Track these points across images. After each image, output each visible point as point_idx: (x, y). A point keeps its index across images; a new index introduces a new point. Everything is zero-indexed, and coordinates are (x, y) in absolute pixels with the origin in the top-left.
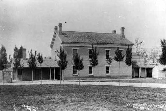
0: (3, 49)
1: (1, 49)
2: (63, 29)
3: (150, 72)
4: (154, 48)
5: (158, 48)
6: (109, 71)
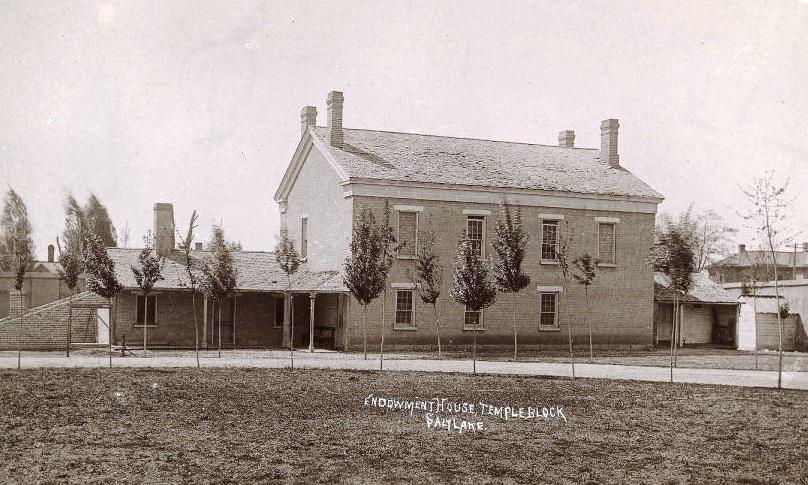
0: (16, 203)
1: (5, 200)
2: (349, 121)
3: (726, 324)
4: (702, 214)
5: (720, 218)
6: (413, 310)
